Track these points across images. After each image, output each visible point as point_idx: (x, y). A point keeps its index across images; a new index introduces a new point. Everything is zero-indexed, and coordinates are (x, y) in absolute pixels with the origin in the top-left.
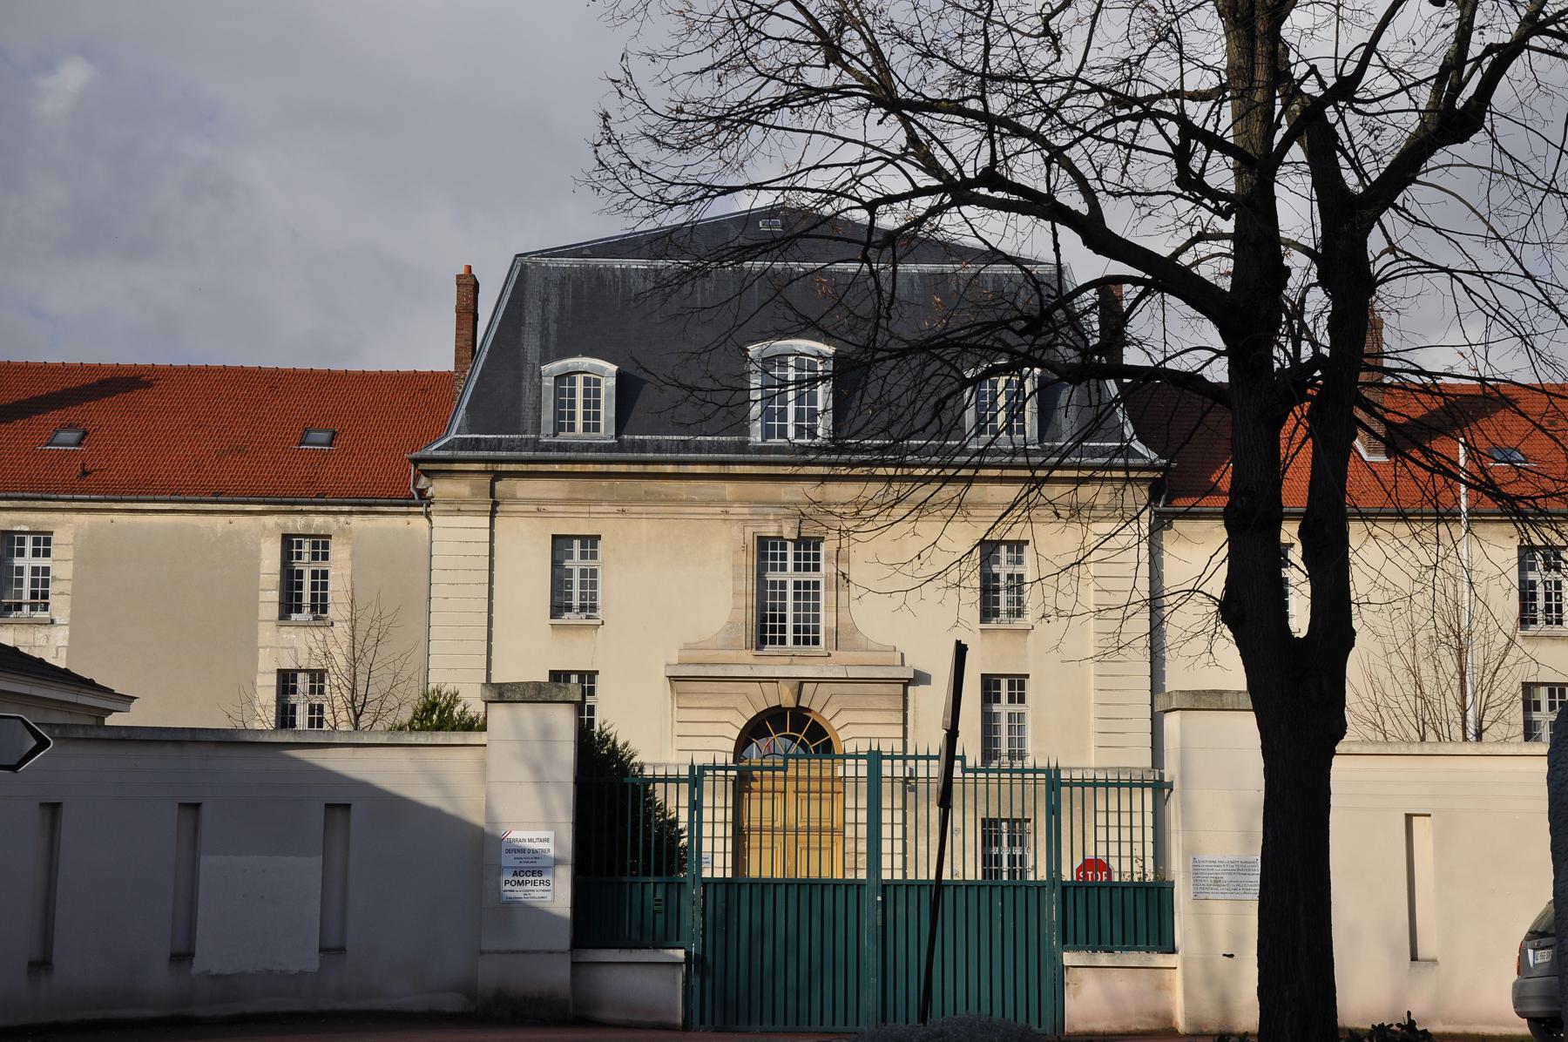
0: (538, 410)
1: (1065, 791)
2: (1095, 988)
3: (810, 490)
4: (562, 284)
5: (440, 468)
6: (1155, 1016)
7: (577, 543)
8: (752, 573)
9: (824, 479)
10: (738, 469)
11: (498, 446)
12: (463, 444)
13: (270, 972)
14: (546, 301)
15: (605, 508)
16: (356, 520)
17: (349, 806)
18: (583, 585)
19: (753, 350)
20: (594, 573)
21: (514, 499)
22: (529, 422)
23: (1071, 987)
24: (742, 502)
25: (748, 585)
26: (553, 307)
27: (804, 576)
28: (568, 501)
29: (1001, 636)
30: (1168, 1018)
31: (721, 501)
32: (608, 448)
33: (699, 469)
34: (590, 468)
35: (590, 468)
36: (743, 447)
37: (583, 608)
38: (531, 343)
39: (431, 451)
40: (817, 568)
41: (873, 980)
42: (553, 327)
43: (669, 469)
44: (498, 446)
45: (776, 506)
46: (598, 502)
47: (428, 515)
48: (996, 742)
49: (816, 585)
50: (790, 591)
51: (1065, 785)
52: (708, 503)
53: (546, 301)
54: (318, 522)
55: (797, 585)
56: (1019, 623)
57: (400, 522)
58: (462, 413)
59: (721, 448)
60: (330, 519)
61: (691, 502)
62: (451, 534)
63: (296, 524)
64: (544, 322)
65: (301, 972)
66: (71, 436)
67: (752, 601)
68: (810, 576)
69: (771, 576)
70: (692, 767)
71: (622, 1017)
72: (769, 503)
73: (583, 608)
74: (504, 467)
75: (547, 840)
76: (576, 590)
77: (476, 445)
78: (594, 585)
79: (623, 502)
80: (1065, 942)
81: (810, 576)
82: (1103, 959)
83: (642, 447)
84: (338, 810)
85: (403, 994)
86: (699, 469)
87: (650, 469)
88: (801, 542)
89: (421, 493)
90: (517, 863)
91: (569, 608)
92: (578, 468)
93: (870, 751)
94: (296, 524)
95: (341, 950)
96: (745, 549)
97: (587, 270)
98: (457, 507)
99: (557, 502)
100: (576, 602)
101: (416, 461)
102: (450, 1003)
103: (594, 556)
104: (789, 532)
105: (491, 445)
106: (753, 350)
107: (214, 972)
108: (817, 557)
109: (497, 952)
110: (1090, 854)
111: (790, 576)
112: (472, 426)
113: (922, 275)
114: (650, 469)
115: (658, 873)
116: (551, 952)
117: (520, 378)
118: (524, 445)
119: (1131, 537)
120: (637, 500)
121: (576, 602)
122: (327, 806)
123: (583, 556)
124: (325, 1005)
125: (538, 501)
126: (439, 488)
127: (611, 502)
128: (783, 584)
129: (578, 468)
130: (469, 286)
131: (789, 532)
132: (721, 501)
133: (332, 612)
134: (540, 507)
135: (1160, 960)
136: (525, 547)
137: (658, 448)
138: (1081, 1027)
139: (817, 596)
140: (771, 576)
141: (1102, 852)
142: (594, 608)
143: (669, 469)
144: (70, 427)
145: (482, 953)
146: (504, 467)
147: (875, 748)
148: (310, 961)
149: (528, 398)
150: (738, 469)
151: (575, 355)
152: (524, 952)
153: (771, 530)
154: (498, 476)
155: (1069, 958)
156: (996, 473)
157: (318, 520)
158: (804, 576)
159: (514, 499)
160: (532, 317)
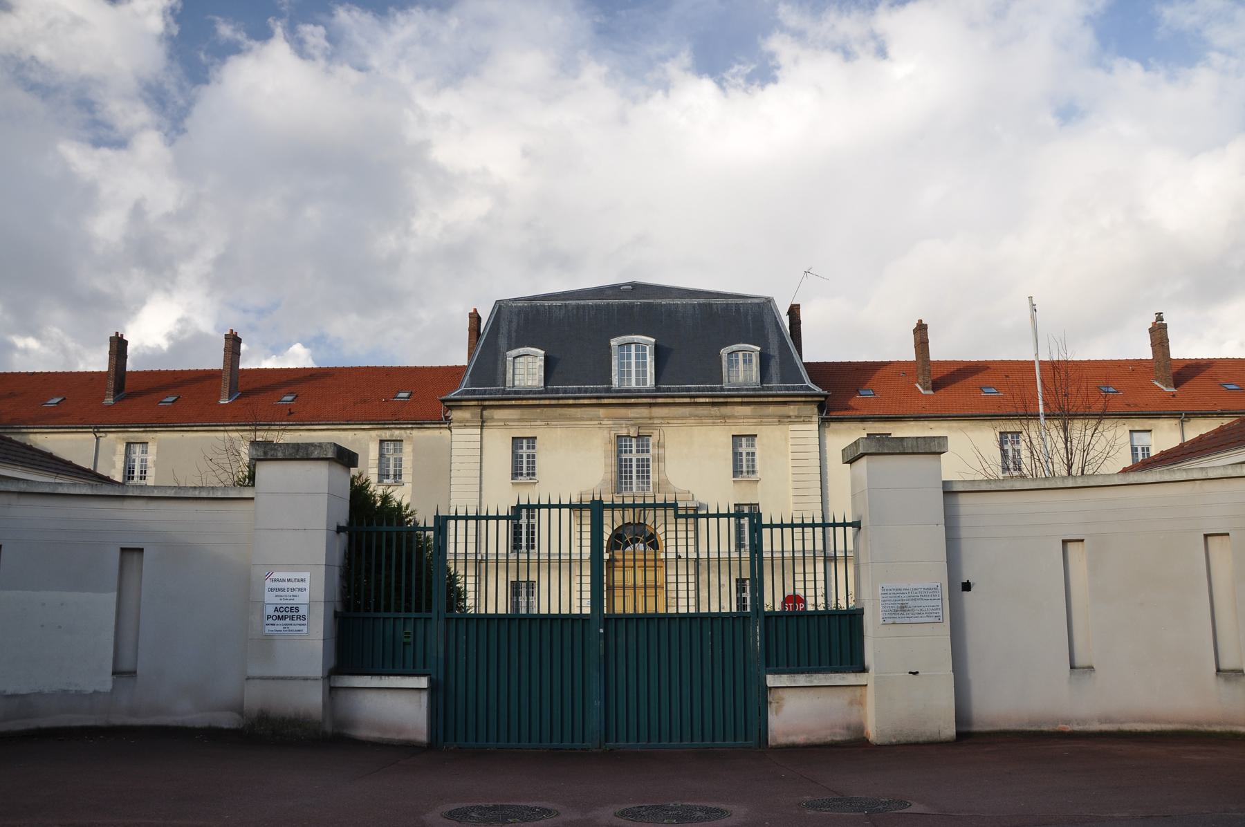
0: (505, 374)
1: (766, 532)
2: (800, 708)
3: (644, 412)
4: (519, 314)
5: (455, 405)
6: (848, 728)
7: (525, 441)
8: (614, 455)
9: (650, 405)
10: (606, 401)
11: (485, 392)
12: (467, 392)
13: (65, 692)
14: (510, 322)
15: (538, 423)
16: (415, 433)
17: (141, 550)
18: (528, 462)
19: (614, 342)
20: (534, 456)
21: (492, 419)
22: (500, 381)
23: (774, 705)
24: (609, 418)
25: (614, 461)
26: (514, 325)
27: (641, 456)
28: (519, 420)
29: (743, 484)
30: (861, 728)
31: (598, 418)
32: (540, 392)
33: (586, 401)
34: (531, 402)
35: (531, 402)
36: (609, 390)
37: (528, 474)
38: (503, 342)
39: (451, 396)
40: (648, 451)
41: (597, 703)
42: (514, 335)
43: (571, 402)
44: (485, 392)
45: (626, 420)
46: (535, 420)
47: (450, 429)
48: (743, 539)
49: (648, 460)
50: (634, 463)
51: (766, 526)
52: (591, 419)
53: (510, 322)
54: (397, 433)
55: (638, 460)
56: (753, 478)
57: (437, 432)
58: (467, 377)
59: (597, 391)
60: (403, 432)
61: (582, 419)
62: (461, 438)
63: (386, 434)
64: (509, 332)
65: (95, 692)
66: (290, 398)
67: (615, 469)
68: (645, 456)
69: (624, 456)
70: (437, 518)
71: (374, 735)
72: (622, 419)
73: (528, 474)
74: (487, 403)
75: (303, 580)
76: (525, 465)
77: (474, 392)
78: (534, 462)
79: (548, 420)
80: (767, 665)
81: (645, 456)
82: (802, 680)
83: (557, 391)
84: (130, 553)
85: (186, 713)
86: (586, 401)
87: (561, 402)
88: (639, 437)
89: (447, 418)
90: (277, 600)
91: (521, 474)
92: (524, 402)
93: (593, 501)
94: (386, 434)
95: (132, 673)
96: (611, 442)
97: (531, 306)
98: (464, 424)
99: (514, 420)
100: (525, 471)
101: (443, 401)
102: (227, 720)
103: (534, 448)
104: (633, 433)
105: (480, 392)
106: (614, 342)
107: (10, 691)
108: (648, 446)
109: (261, 678)
110: (789, 591)
111: (634, 456)
112: (472, 384)
113: (699, 304)
114: (561, 402)
115: (418, 609)
116: (306, 679)
117: (497, 360)
118: (497, 392)
119: (811, 429)
120: (555, 418)
121: (525, 471)
122: (123, 550)
123: (528, 448)
124: (117, 721)
125: (505, 420)
126: (455, 415)
127: (542, 420)
128: (631, 460)
129: (524, 402)
130: (475, 318)
131: (633, 433)
132: (598, 418)
133: (404, 479)
134: (506, 423)
135: (851, 679)
136: (498, 443)
137: (565, 391)
138: (782, 740)
139: (648, 466)
140: (624, 456)
141: (800, 593)
142: (534, 474)
143: (571, 402)
144: (290, 394)
145: (248, 679)
146: (487, 403)
147: (597, 498)
148: (105, 682)
149: (500, 369)
150: (606, 401)
151: (523, 346)
152: (282, 678)
153: (624, 432)
154: (484, 408)
155: (771, 680)
156: (739, 400)
157: (397, 432)
158: (641, 456)
159: (492, 419)
160: (504, 329)
